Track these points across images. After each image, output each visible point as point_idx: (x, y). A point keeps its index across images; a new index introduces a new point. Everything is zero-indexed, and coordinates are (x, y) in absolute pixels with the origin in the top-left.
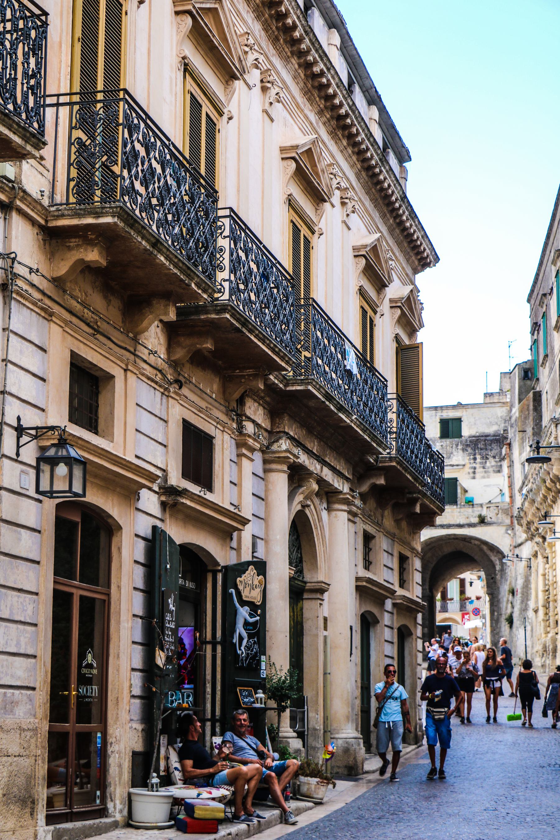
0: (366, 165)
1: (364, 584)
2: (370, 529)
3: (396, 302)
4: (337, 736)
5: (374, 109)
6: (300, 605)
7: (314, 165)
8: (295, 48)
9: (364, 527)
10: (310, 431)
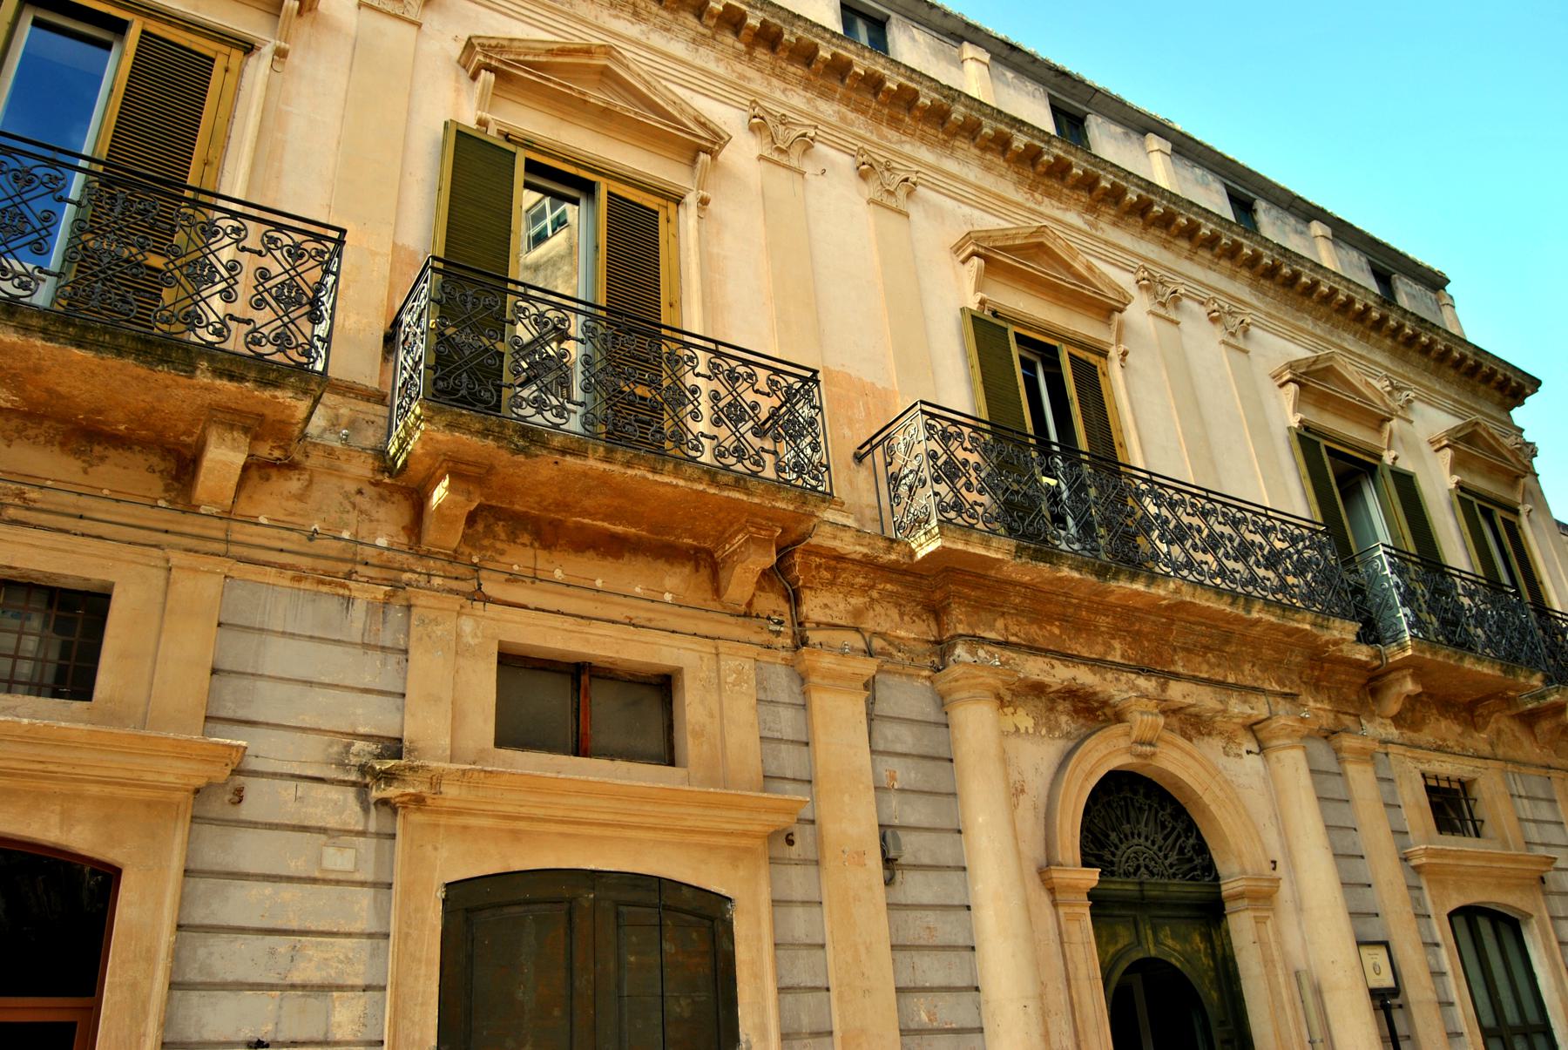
1: (1424, 860)
2: (1448, 768)
3: (1439, 441)
5: (1154, 142)
6: (1223, 925)
8: (1217, 250)
9: (1422, 767)
10: (1235, 662)
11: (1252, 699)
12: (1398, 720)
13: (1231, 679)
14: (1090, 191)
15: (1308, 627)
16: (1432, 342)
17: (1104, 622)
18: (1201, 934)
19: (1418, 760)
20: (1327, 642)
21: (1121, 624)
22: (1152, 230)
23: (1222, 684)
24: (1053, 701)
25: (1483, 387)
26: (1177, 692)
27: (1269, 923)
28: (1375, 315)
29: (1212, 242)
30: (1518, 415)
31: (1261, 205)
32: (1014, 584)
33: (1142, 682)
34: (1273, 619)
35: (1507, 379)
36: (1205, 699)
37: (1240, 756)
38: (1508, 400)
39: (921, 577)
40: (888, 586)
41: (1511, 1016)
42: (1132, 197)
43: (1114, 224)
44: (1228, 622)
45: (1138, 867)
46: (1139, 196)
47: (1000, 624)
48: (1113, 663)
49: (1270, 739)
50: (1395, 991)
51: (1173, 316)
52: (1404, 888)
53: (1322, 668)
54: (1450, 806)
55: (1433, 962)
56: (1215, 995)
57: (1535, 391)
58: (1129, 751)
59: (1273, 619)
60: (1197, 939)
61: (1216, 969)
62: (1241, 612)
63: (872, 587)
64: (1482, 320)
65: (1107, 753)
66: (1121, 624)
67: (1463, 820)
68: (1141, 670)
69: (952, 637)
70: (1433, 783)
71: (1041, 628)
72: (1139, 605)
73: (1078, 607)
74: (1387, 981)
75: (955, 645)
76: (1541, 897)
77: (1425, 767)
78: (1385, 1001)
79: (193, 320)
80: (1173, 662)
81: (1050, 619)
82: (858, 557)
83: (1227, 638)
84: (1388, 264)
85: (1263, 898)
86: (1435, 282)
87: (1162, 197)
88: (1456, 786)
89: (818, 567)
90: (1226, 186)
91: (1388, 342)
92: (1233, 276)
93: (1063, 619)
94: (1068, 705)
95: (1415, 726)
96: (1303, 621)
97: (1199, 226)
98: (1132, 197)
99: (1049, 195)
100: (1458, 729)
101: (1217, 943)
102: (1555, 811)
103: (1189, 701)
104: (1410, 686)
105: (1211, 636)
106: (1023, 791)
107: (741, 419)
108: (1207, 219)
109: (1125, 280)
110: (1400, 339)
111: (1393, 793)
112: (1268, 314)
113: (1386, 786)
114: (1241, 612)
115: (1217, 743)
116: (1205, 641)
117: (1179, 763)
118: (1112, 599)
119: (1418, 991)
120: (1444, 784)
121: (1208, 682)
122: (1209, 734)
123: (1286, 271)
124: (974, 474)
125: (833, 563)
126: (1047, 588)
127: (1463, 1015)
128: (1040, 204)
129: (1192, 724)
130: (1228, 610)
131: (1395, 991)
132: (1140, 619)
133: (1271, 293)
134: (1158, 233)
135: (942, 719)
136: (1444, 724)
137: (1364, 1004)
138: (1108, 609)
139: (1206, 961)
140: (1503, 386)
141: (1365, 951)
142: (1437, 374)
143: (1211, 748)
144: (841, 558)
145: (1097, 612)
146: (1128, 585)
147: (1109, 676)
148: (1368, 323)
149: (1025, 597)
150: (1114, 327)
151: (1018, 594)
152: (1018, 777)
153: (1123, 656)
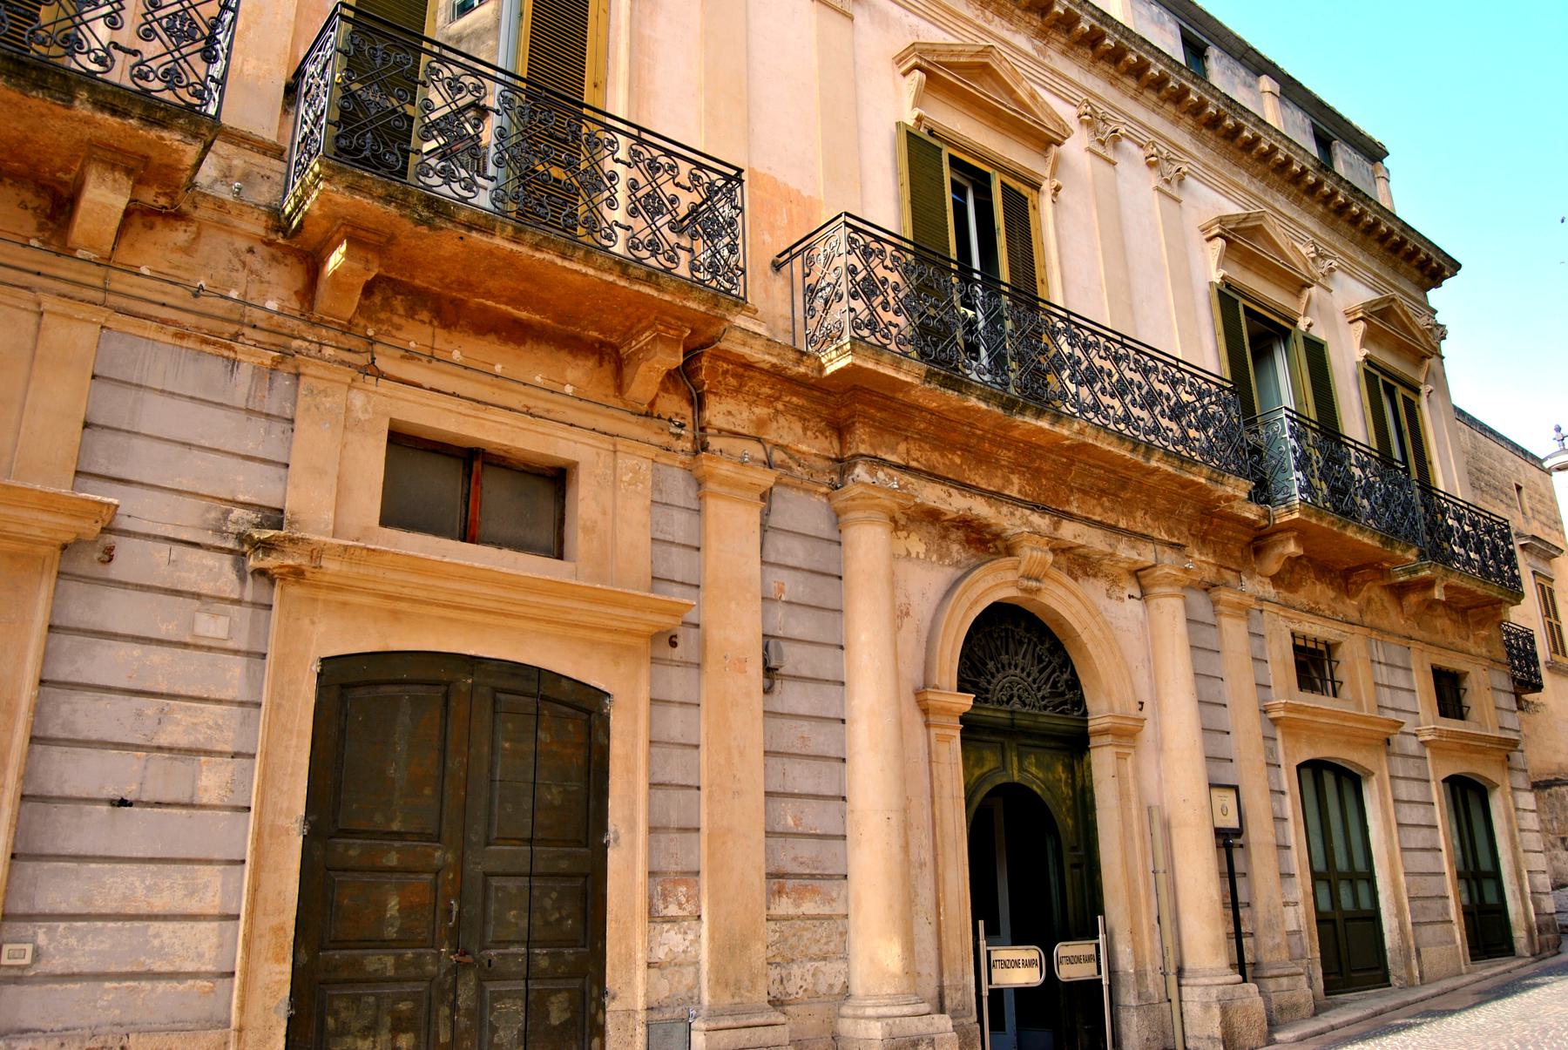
0: (1387, 244)
1: (1282, 714)
2: (1317, 629)
3: (1354, 313)
4: (1192, 981)
7: (1011, 93)
8: (1163, 93)
9: (1292, 626)
10: (1128, 508)
11: (1140, 545)
12: (1276, 580)
13: (1122, 524)
14: (1043, 16)
15: (1203, 481)
16: (1363, 213)
17: (1005, 456)
18: (1064, 766)
19: (1290, 619)
20: (1220, 498)
21: (1021, 460)
22: (1100, 64)
23: (1113, 528)
24: (946, 529)
25: (1404, 265)
26: (1069, 531)
27: (1129, 759)
28: (1311, 179)
29: (1159, 84)
30: (1434, 297)
31: (1213, 52)
32: (920, 409)
33: (1035, 518)
34: (1170, 469)
35: (1429, 259)
36: (1094, 540)
37: (1121, 599)
38: (1427, 280)
39: (829, 393)
40: (795, 400)
41: (1341, 863)
42: (1084, 26)
43: (1063, 53)
44: (1126, 468)
45: (1012, 697)
46: (1092, 27)
47: (902, 447)
48: (1010, 497)
49: (1153, 585)
50: (1238, 833)
51: (1111, 156)
52: (1260, 738)
53: (1211, 523)
54: (1313, 665)
55: (1277, 808)
56: (1070, 822)
57: (1453, 274)
58: (1015, 584)
59: (1170, 469)
60: (1060, 769)
61: (1074, 799)
62: (1140, 459)
63: (778, 399)
64: (1413, 197)
65: (995, 584)
66: (1021, 460)
67: (1323, 680)
68: (1035, 507)
69: (854, 456)
70: (1300, 642)
71: (943, 456)
72: (1042, 443)
73: (982, 438)
74: (1232, 822)
75: (855, 465)
76: (1384, 758)
77: (1296, 627)
78: (1228, 841)
79: (73, 44)
80: (1068, 502)
81: (953, 448)
82: (766, 366)
83: (1124, 484)
84: (1331, 128)
85: (1127, 734)
86: (1373, 153)
87: (1116, 31)
88: (1321, 647)
89: (725, 372)
90: (1181, 27)
91: (1320, 208)
92: (1175, 122)
93: (966, 449)
94: (961, 534)
95: (1292, 587)
96: (1200, 474)
97: (1148, 65)
98: (1084, 26)
99: (1000, 15)
100: (1331, 594)
101: (1078, 774)
102: (1410, 680)
103: (1079, 541)
104: (1292, 548)
105: (1108, 480)
106: (907, 614)
107: (658, 212)
108: (1157, 59)
109: (1068, 113)
110: (1331, 206)
111: (1262, 648)
112: (1206, 166)
113: (1256, 641)
114: (1140, 459)
115: (1101, 585)
116: (1102, 484)
117: (1063, 600)
118: (1016, 434)
119: (1259, 834)
120: (1311, 645)
121: (1100, 525)
122: (1095, 576)
123: (1229, 122)
124: (892, 294)
125: (740, 370)
126: (953, 416)
127: (1297, 859)
128: (989, 22)
129: (1079, 563)
130: (1129, 455)
131: (1238, 833)
132: (1041, 457)
133: (1212, 144)
134: (1106, 67)
135: (835, 536)
136: (1319, 587)
137: (1209, 840)
138: (1009, 443)
139: (1066, 790)
140: (1424, 265)
141: (1216, 793)
142: (1363, 246)
143: (1094, 590)
144: (749, 366)
145: (1000, 446)
146: (1033, 422)
147: (1005, 510)
148: (1303, 186)
149: (930, 423)
150: (1050, 160)
151: (924, 420)
152: (904, 600)
153: (1020, 492)
